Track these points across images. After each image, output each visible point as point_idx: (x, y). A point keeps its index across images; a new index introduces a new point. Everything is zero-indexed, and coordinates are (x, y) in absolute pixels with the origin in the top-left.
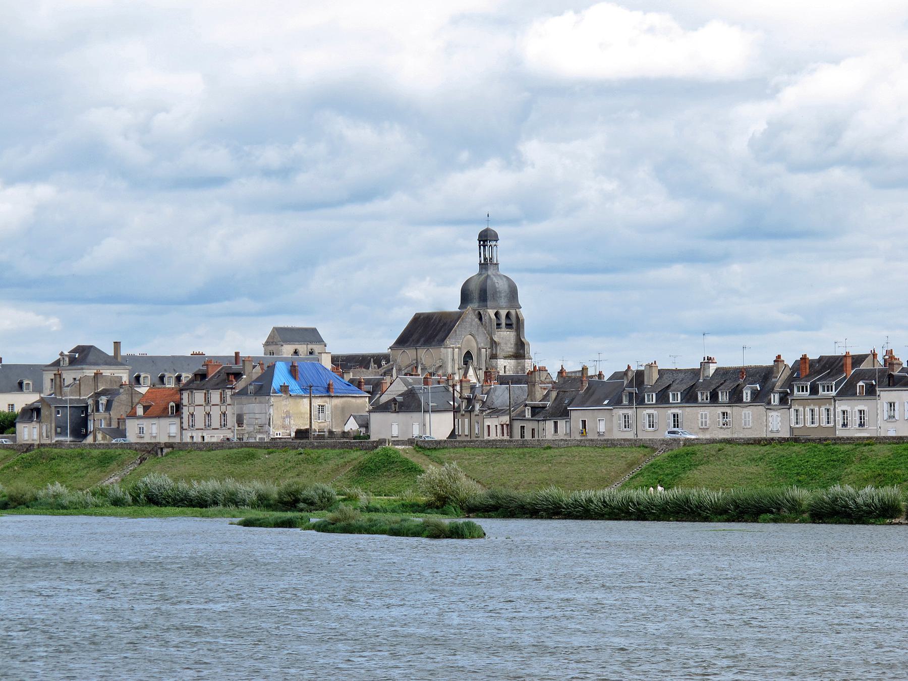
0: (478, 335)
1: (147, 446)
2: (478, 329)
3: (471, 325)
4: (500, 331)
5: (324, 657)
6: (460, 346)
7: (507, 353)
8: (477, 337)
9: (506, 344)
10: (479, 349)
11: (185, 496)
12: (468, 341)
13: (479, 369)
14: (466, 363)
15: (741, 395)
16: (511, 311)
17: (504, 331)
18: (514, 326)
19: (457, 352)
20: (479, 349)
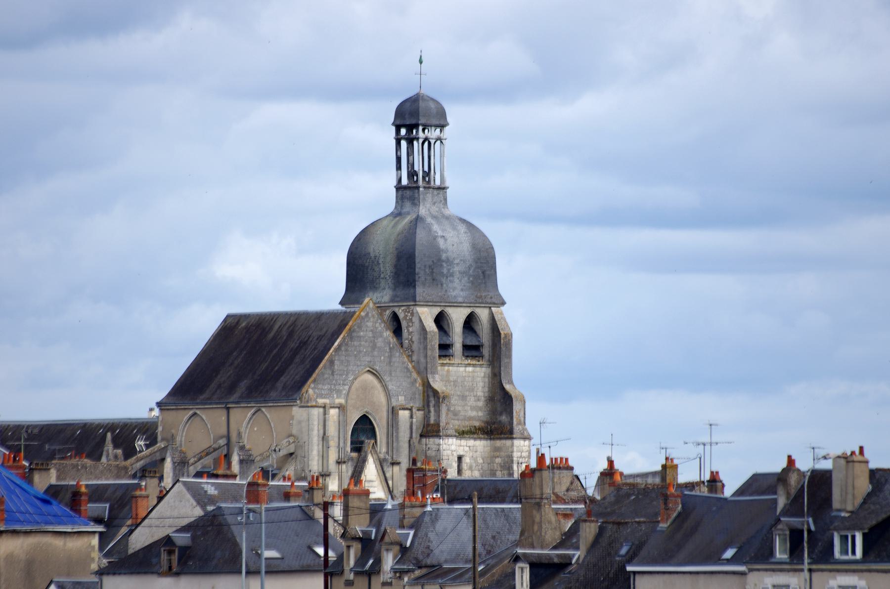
0: (391, 374)
2: (390, 357)
3: (374, 347)
4: (450, 365)
8: (386, 378)
10: (393, 412)
13: (393, 464)
14: (357, 447)
17: (458, 365)
18: (486, 351)
20: (393, 412)
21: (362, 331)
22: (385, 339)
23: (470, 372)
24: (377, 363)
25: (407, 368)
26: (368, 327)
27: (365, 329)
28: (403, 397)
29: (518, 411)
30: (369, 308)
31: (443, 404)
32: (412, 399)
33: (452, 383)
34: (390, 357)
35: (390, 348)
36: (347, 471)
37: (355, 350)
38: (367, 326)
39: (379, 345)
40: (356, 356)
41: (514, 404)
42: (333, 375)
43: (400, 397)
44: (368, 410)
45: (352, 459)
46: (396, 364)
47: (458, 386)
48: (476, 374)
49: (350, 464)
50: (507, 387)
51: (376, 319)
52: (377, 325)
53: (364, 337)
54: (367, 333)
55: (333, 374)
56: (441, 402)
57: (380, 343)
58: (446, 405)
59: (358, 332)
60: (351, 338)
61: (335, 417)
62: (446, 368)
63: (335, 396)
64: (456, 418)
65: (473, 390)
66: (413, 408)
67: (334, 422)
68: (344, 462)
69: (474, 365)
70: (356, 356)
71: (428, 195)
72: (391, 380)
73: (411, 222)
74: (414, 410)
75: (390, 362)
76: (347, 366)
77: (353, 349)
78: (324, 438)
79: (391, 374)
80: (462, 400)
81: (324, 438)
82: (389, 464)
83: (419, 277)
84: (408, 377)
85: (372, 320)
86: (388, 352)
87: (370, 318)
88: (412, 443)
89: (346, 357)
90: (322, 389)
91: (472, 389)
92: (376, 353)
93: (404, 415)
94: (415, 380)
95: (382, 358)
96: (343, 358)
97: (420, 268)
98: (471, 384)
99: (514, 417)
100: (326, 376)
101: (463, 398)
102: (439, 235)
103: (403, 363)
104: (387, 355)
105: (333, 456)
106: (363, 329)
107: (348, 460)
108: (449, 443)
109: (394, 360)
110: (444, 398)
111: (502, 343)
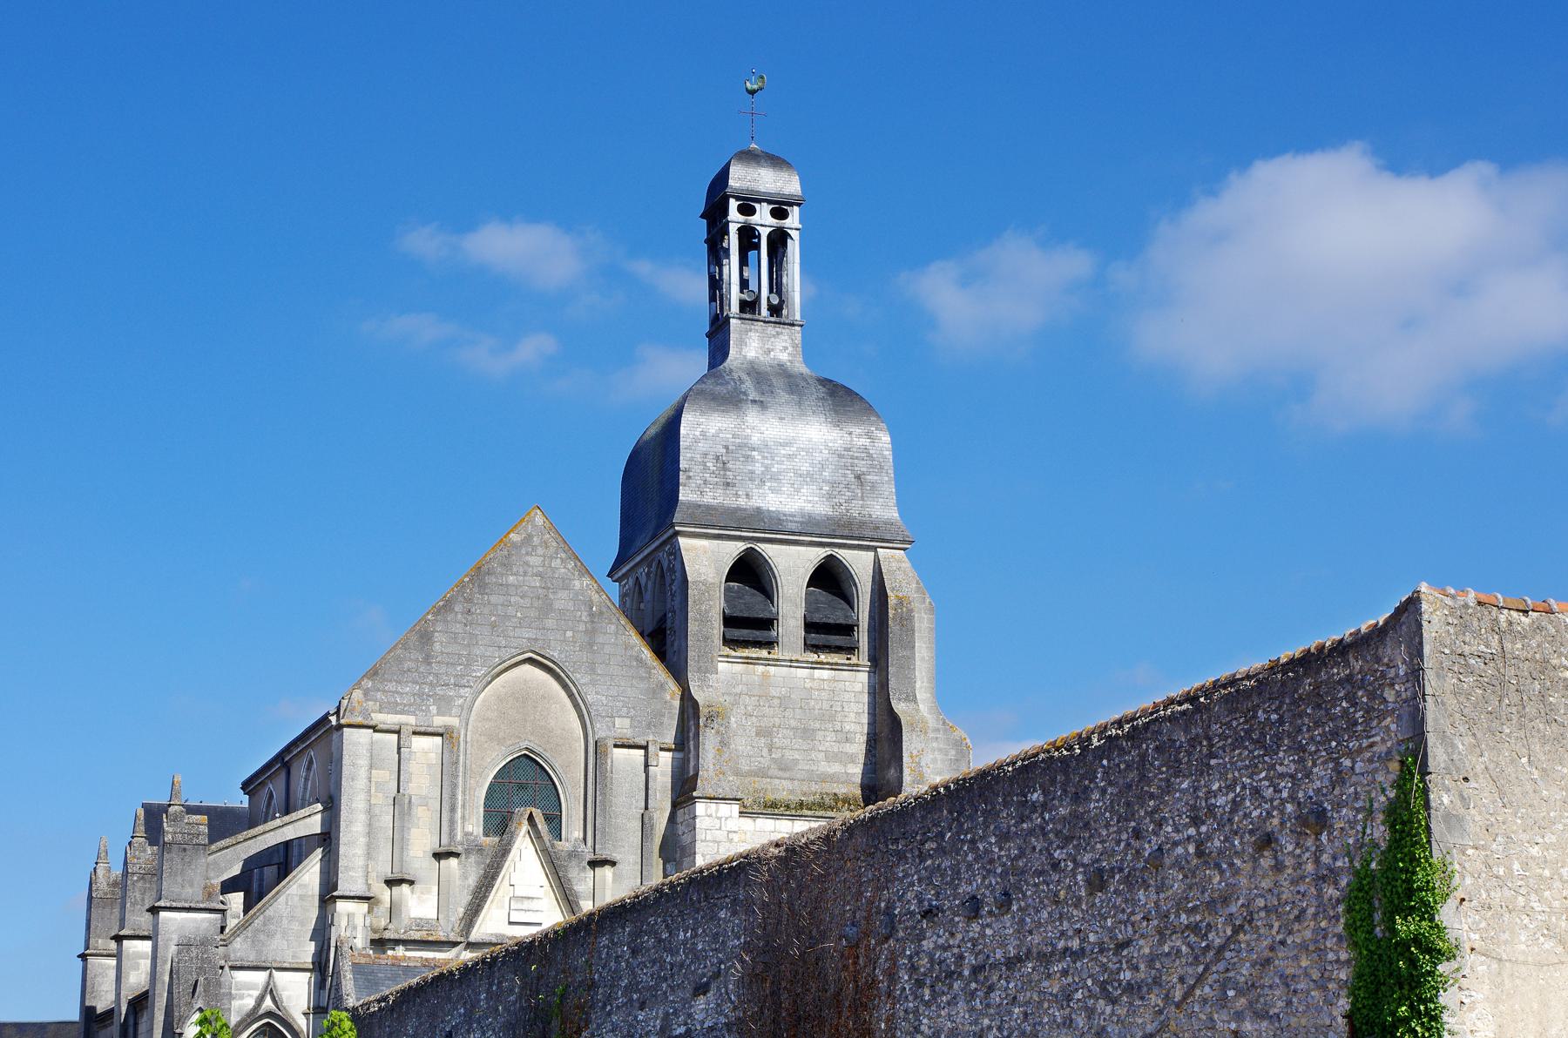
0: (593, 670)
1: (678, 599)
2: (591, 633)
3: (546, 609)
4: (768, 662)
5: (222, 932)
6: (453, 721)
7: (814, 787)
8: (581, 678)
9: (807, 733)
10: (597, 752)
11: (809, 517)
12: (523, 698)
13: (594, 864)
14: (499, 822)
15: (898, 753)
16: (844, 555)
17: (792, 663)
18: (863, 638)
19: (434, 758)
20: (597, 752)
21: (512, 575)
22: (577, 594)
23: (824, 680)
24: (552, 643)
25: (639, 660)
26: (529, 566)
27: (521, 570)
28: (627, 722)
29: (915, 752)
30: (534, 526)
31: (708, 730)
32: (654, 724)
33: (776, 702)
34: (591, 633)
35: (591, 615)
36: (465, 877)
37: (491, 614)
38: (527, 564)
39: (558, 605)
40: (493, 626)
41: (904, 738)
42: (430, 664)
43: (617, 721)
44: (532, 745)
45: (480, 850)
46: (607, 649)
47: (794, 709)
48: (841, 685)
49: (472, 859)
50: (899, 707)
51: (552, 550)
52: (556, 563)
53: (517, 587)
54: (526, 578)
55: (427, 660)
56: (701, 724)
57: (562, 600)
58: (718, 732)
59: (502, 575)
60: (479, 586)
61: (433, 755)
62: (760, 669)
63: (433, 709)
64: (787, 775)
65: (832, 719)
66: (650, 743)
67: (430, 766)
68: (457, 855)
69: (834, 667)
70: (493, 626)
71: (752, 334)
72: (593, 683)
73: (781, 419)
74: (651, 748)
75: (591, 645)
76: (469, 645)
77: (486, 611)
78: (400, 804)
79: (593, 670)
80: (802, 738)
81: (400, 804)
82: (585, 863)
83: (689, 477)
84: (642, 679)
85: (540, 551)
86: (586, 623)
87: (534, 548)
88: (646, 820)
89: (466, 625)
90: (398, 693)
91: (829, 717)
92: (550, 623)
93: (626, 761)
94: (662, 686)
95: (569, 634)
96: (458, 628)
97: (692, 459)
98: (826, 706)
99: (905, 765)
100: (407, 665)
101: (807, 733)
102: (750, 398)
103: (627, 647)
104: (582, 627)
105: (422, 841)
106: (515, 570)
107: (468, 852)
108: (719, 815)
109: (600, 639)
110: (710, 718)
111: (890, 615)
